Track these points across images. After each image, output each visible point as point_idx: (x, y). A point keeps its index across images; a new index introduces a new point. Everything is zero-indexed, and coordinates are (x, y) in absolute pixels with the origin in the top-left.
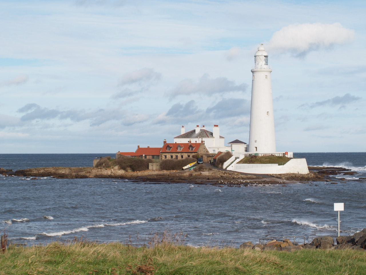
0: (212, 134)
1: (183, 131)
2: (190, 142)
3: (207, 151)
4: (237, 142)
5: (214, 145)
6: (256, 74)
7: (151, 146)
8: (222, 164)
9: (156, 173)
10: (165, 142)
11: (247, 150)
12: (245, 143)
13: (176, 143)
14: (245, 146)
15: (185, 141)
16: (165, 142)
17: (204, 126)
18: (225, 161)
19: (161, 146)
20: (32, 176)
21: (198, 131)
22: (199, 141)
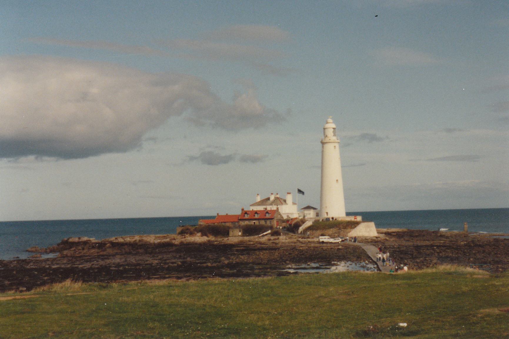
0: (285, 201)
1: (259, 199)
2: (266, 209)
3: (282, 217)
4: (308, 208)
5: (287, 211)
6: (326, 146)
7: (230, 214)
8: (298, 229)
9: (241, 239)
10: (243, 210)
11: (317, 215)
12: (314, 209)
13: (218, 214)
14: (316, 211)
15: (261, 208)
16: (243, 210)
17: (277, 194)
18: (300, 226)
19: (239, 213)
20: (309, 228)
21: (272, 198)
22: (274, 208)
